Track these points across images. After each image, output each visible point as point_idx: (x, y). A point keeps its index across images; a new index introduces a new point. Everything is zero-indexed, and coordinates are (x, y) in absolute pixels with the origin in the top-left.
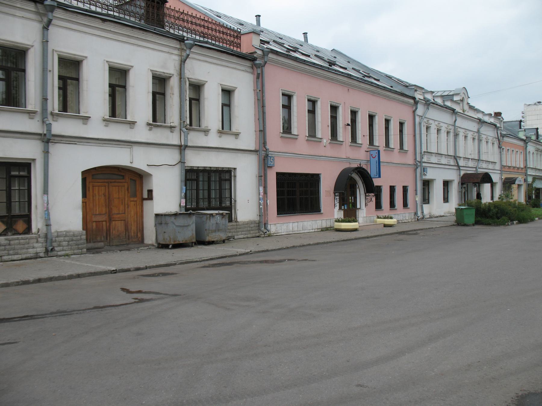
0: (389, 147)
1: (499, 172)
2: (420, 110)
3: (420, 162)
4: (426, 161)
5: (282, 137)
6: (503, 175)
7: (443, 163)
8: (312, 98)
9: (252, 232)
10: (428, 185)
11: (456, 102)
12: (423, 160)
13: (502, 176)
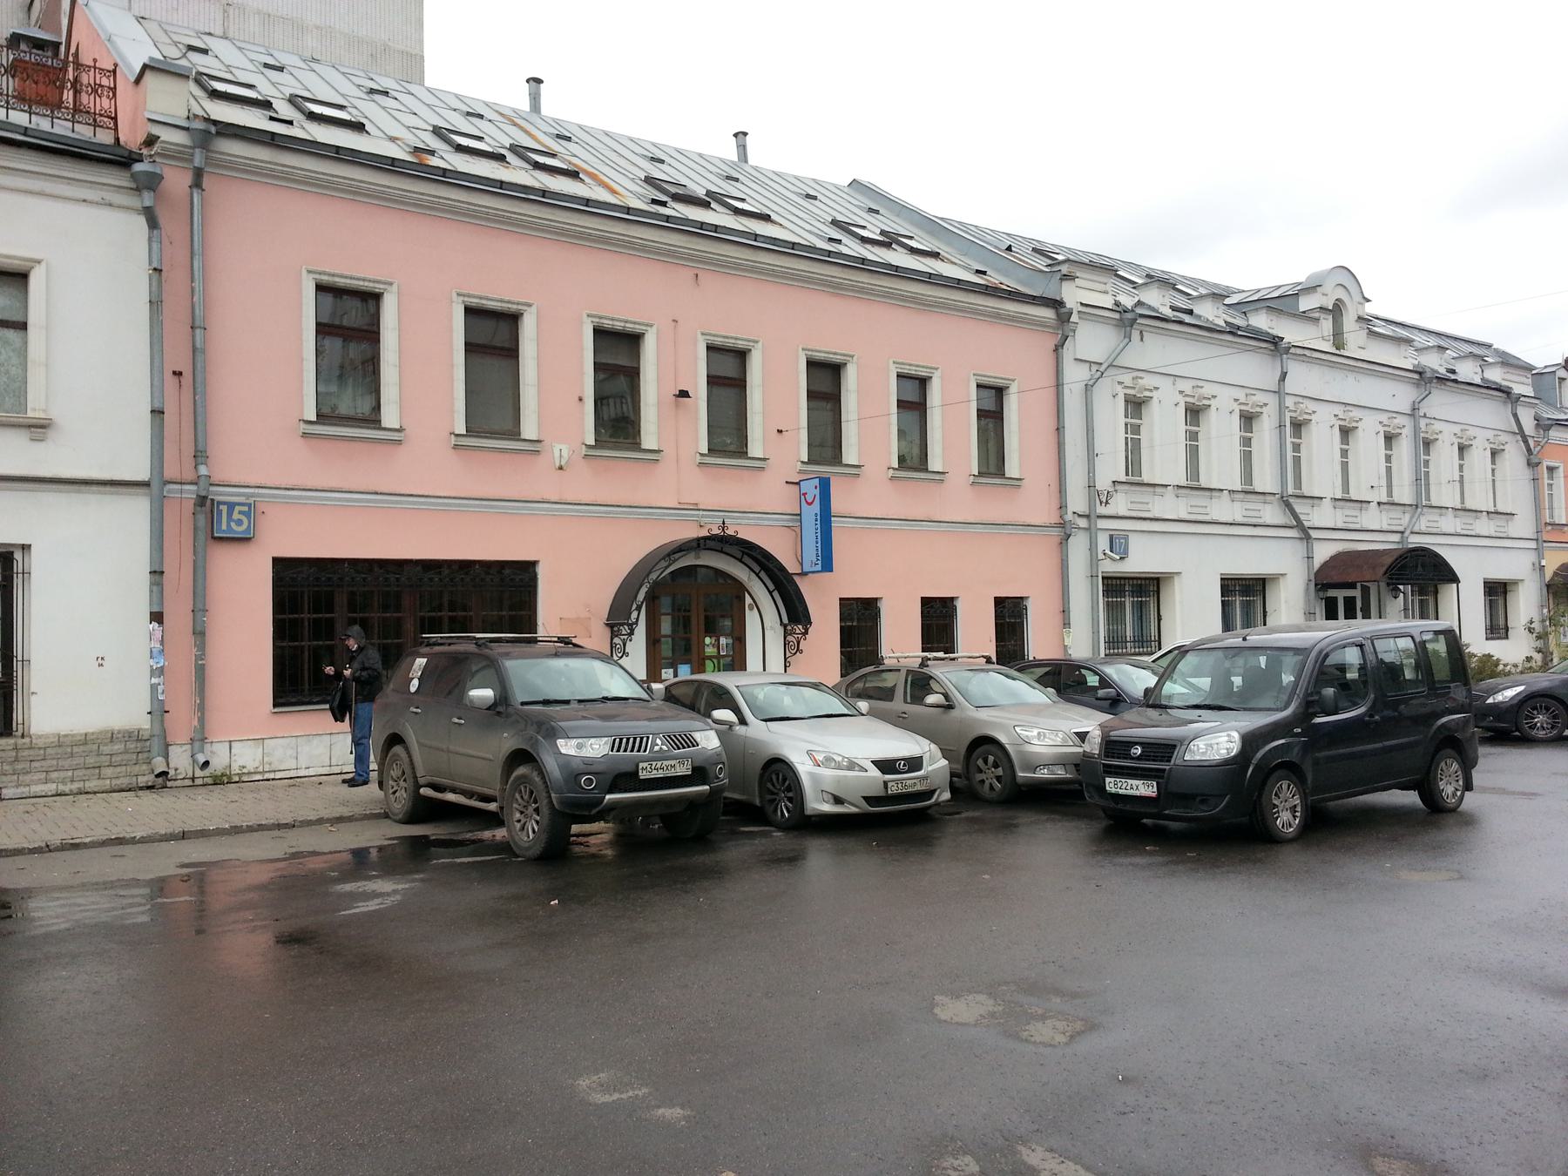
0: (926, 470)
1: (1533, 545)
2: (1091, 341)
3: (1088, 516)
4: (1423, 529)
5: (305, 435)
6: (1547, 553)
7: (1269, 522)
8: (992, 382)
9: (108, 772)
10: (1505, 593)
11: (1306, 317)
12: (1101, 510)
13: (1541, 557)
